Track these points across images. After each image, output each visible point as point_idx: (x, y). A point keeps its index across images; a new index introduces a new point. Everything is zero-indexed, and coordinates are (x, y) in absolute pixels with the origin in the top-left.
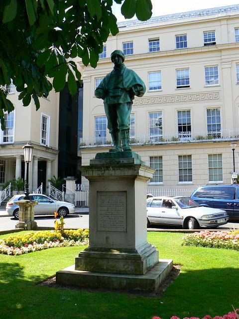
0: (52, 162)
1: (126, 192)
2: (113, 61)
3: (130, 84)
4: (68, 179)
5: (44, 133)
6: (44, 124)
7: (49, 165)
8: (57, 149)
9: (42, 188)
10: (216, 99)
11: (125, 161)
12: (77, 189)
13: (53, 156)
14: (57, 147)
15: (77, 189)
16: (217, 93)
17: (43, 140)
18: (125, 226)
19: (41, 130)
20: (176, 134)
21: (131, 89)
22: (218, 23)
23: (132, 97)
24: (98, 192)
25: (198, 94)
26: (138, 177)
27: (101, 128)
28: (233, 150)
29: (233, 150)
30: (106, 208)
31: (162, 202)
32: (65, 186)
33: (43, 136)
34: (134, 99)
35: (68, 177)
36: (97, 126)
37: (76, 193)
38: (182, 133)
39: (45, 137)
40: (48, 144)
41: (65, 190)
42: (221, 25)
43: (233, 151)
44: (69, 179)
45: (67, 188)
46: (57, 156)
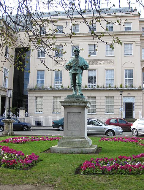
1: (81, 113)
3: (82, 64)
4: (20, 109)
5: (5, 81)
10: (112, 64)
11: (80, 99)
12: (26, 115)
15: (26, 115)
16: (113, 60)
18: (80, 128)
19: (3, 77)
20: (87, 84)
21: (83, 67)
23: (83, 71)
24: (68, 112)
25: (101, 60)
26: (86, 107)
27: (41, 78)
28: (121, 95)
29: (121, 95)
30: (72, 120)
32: (19, 113)
33: (4, 82)
35: (21, 108)
36: (38, 77)
37: (26, 118)
38: (91, 84)
39: (5, 82)
41: (18, 115)
43: (120, 96)
44: (21, 109)
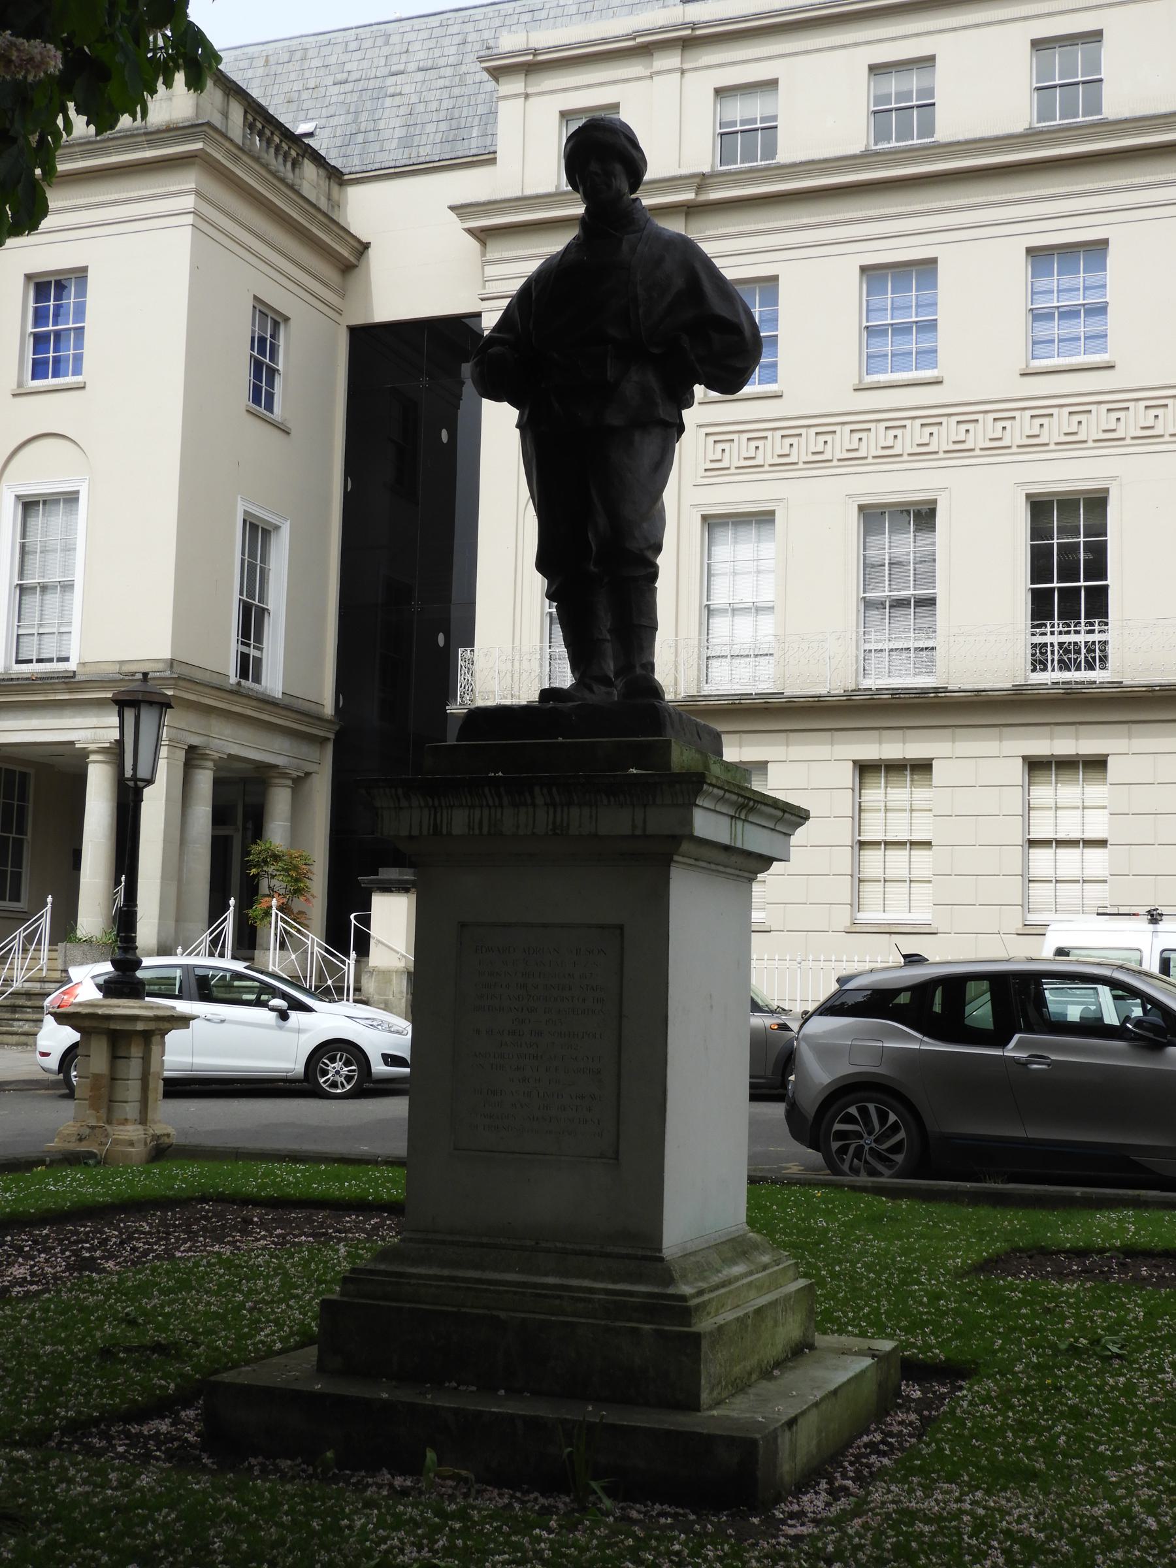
0: (299, 782)
2: (575, 188)
6: (252, 568)
7: (280, 801)
8: (329, 710)
9: (229, 926)
13: (305, 750)
14: (326, 699)
16: (873, 361)
17: (244, 658)
22: (635, 69)
24: (463, 925)
26: (685, 846)
31: (143, 773)
32: (366, 921)
34: (689, 404)
35: (389, 874)
39: (259, 639)
40: (273, 682)
41: (363, 948)
42: (651, 77)
45: (376, 931)
46: (329, 749)
